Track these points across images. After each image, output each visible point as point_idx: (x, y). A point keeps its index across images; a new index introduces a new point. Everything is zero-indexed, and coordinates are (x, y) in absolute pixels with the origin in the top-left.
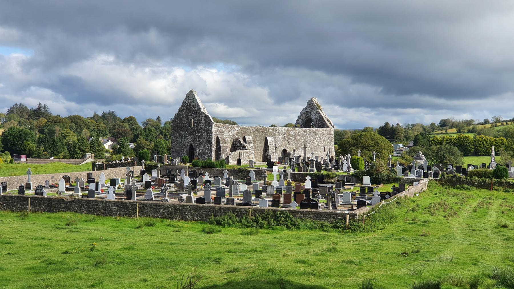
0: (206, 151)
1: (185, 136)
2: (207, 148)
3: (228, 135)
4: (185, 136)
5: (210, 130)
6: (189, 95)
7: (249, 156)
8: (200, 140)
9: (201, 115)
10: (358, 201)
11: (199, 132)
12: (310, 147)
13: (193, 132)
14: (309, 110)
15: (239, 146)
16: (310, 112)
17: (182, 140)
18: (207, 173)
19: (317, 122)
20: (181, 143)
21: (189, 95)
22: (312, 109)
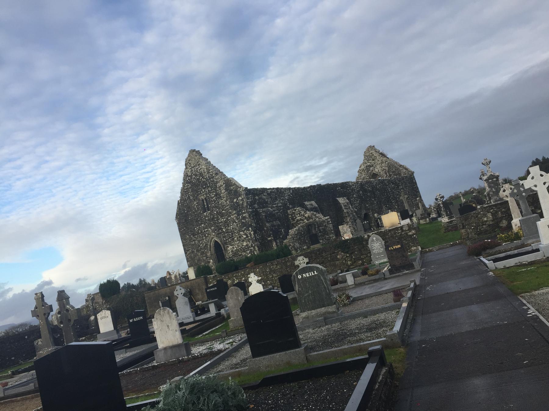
0: (245, 244)
1: (202, 232)
2: (245, 238)
3: (274, 206)
4: (202, 232)
5: (241, 203)
6: (189, 160)
7: (324, 230)
8: (228, 229)
9: (218, 184)
10: (95, 339)
11: (222, 215)
12: (396, 204)
13: (213, 219)
14: (369, 164)
15: (301, 220)
16: (373, 165)
17: (199, 241)
18: (252, 275)
19: (386, 174)
20: (199, 246)
21: (189, 160)
22: (373, 160)
